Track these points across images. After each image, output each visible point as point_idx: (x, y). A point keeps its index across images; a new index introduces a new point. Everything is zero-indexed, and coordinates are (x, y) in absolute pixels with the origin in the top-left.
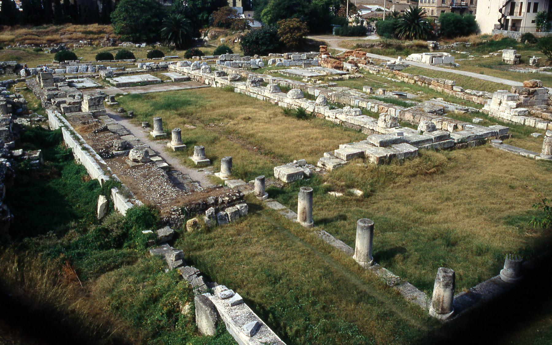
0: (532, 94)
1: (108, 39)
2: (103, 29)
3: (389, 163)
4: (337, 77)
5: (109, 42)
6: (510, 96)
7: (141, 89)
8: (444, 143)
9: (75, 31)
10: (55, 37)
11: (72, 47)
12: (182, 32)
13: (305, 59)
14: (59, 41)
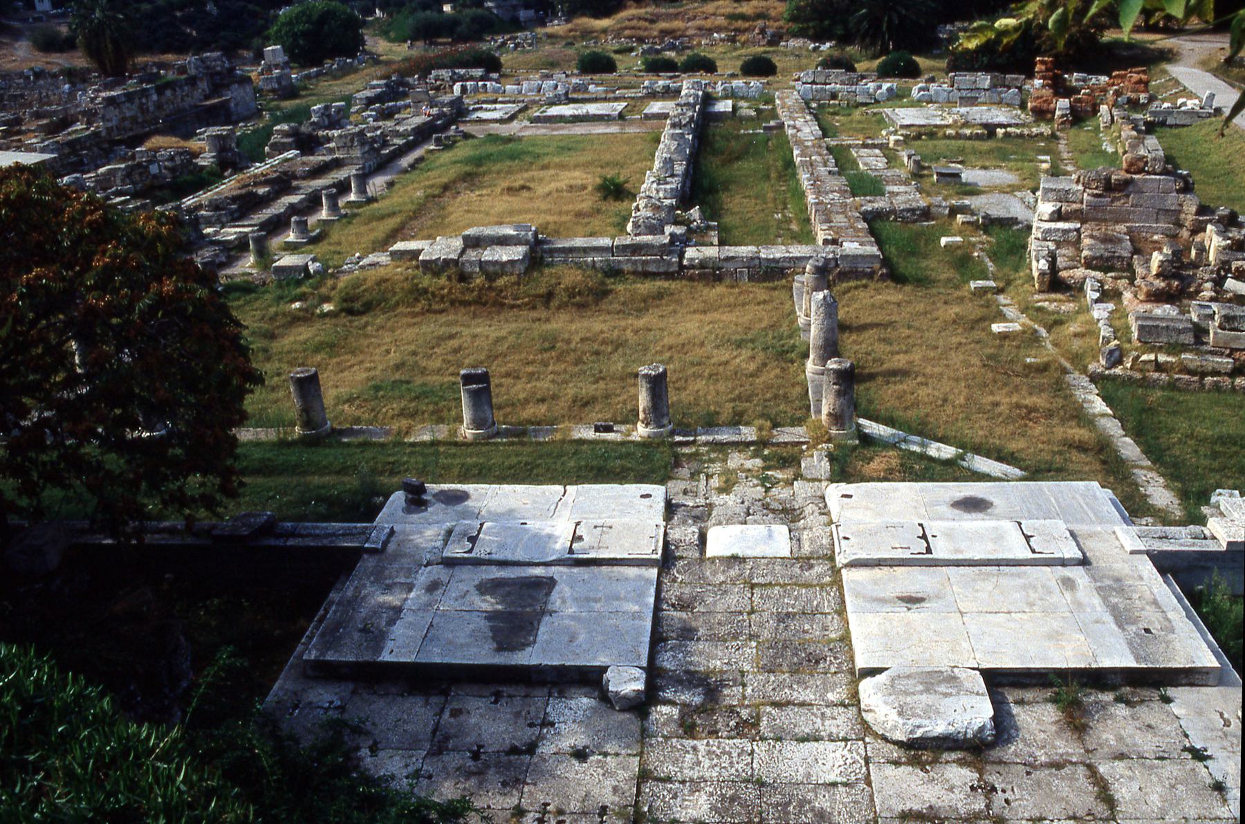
0: (1120, 191)
1: (763, 31)
2: (768, 10)
3: (437, 274)
4: (968, 132)
5: (763, 38)
6: (1052, 190)
7: (546, 128)
8: (645, 263)
9: (714, 14)
10: (677, 24)
11: (699, 44)
12: (890, 22)
13: (986, 87)
14: (679, 33)
